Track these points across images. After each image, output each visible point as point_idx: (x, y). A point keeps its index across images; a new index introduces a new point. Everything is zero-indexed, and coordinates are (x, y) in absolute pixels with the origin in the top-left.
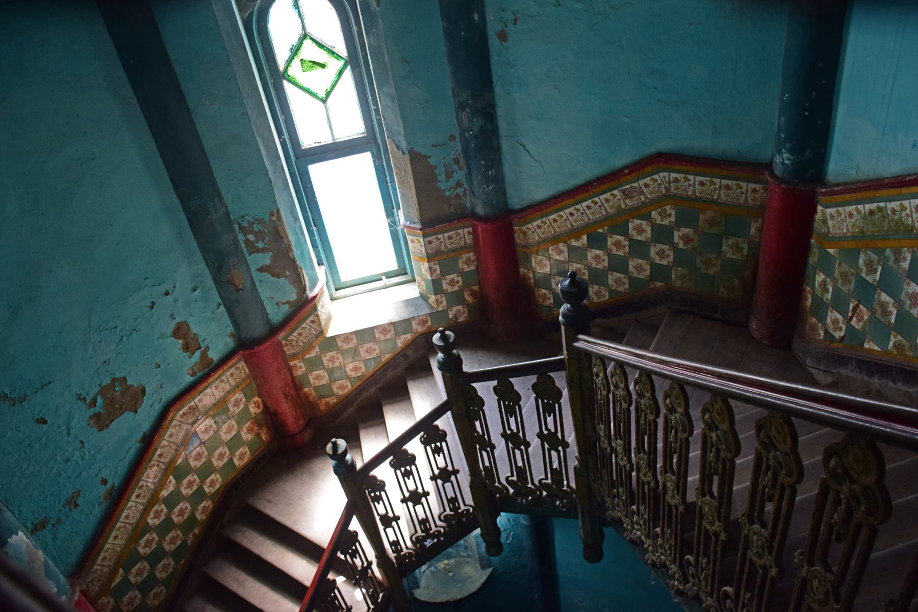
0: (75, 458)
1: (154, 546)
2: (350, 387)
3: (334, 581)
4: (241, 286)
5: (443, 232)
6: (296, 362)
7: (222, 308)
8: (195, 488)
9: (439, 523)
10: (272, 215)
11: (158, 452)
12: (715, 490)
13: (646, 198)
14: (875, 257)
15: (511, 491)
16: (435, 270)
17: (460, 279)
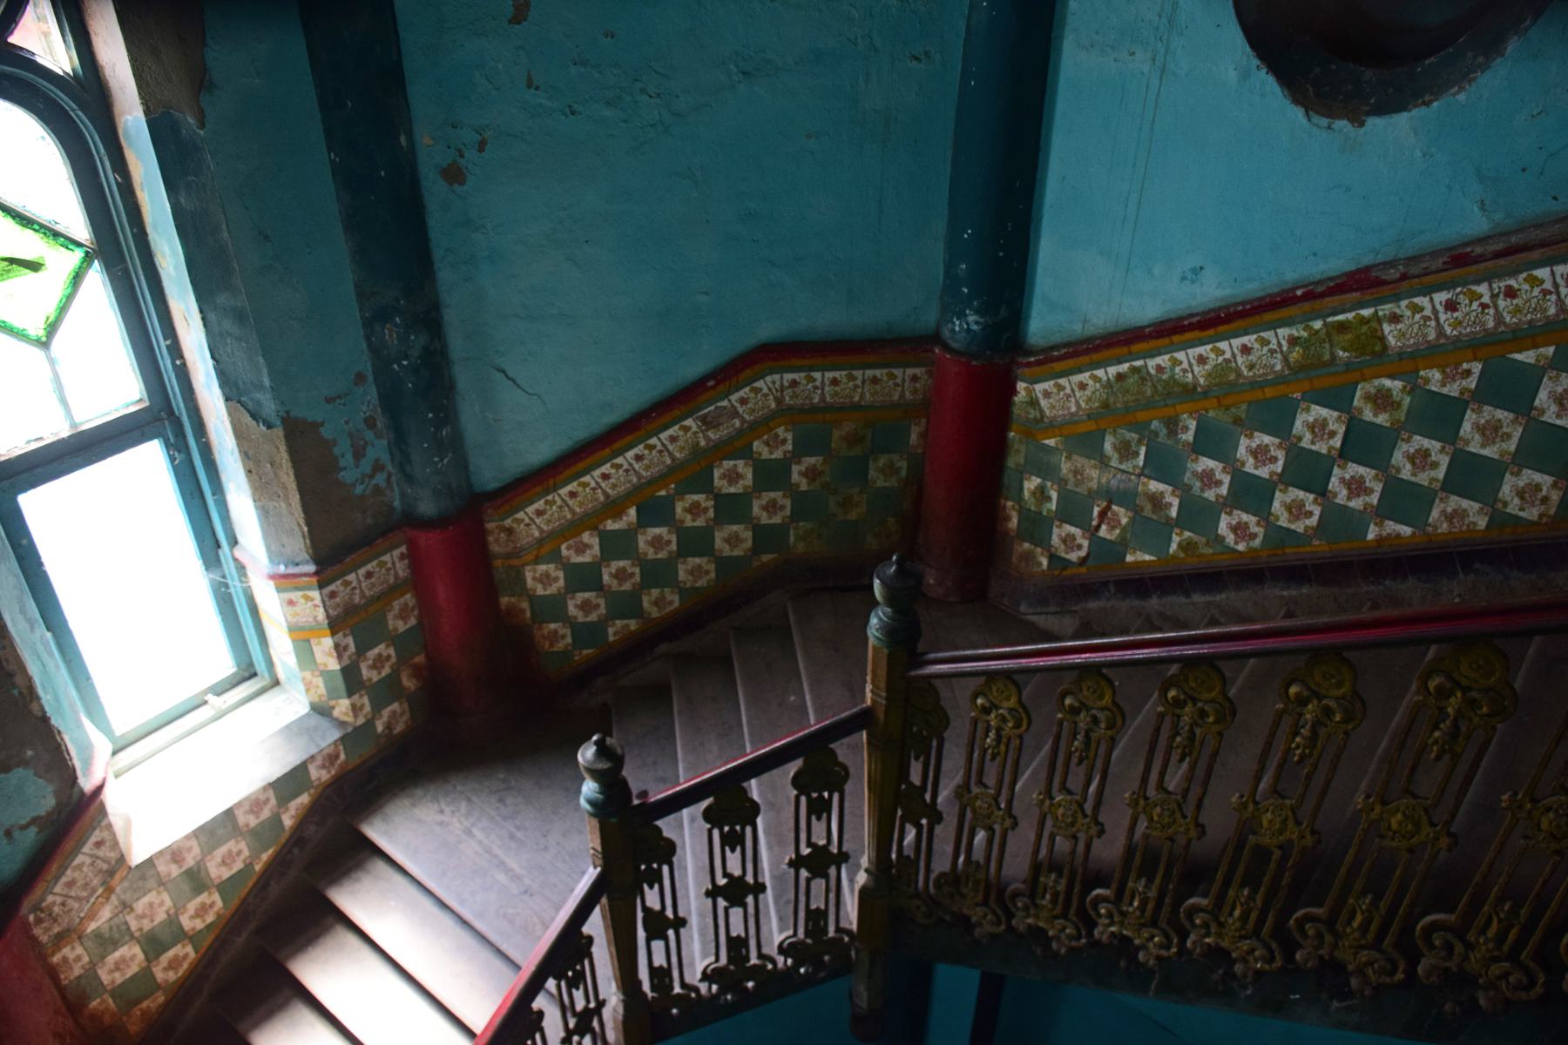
6: (66, 951)
13: (743, 421)
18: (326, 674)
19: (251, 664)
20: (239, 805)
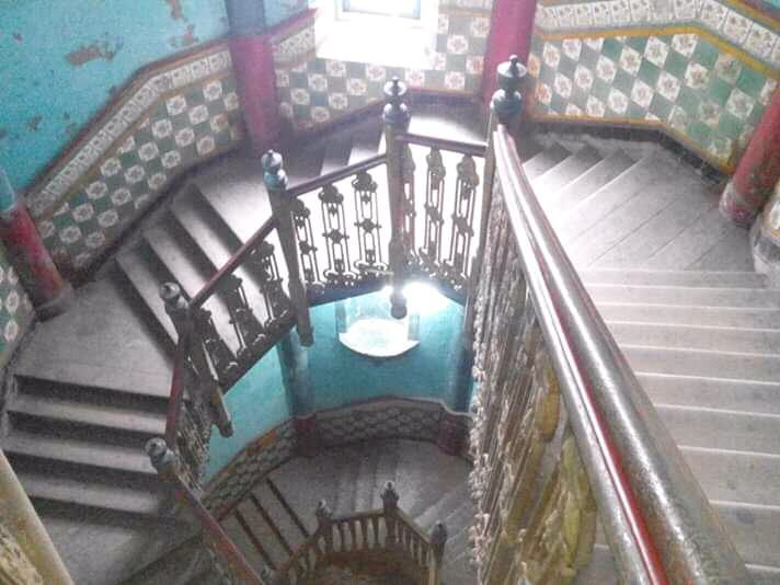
3: (240, 280)
13: (674, 17)
16: (443, 25)
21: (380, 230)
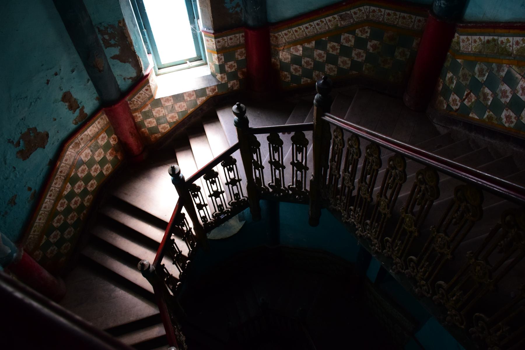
0: (11, 177)
1: (62, 222)
2: (169, 128)
3: (174, 240)
4: (102, 69)
5: (226, 36)
6: (137, 114)
7: (90, 82)
8: (82, 189)
9: (228, 206)
10: (120, 22)
11: (59, 170)
12: (350, 169)
13: (354, 20)
14: (485, 67)
15: (271, 190)
17: (236, 64)
18: (215, 65)
19: (201, 56)
20: (185, 93)
21: (241, 182)
